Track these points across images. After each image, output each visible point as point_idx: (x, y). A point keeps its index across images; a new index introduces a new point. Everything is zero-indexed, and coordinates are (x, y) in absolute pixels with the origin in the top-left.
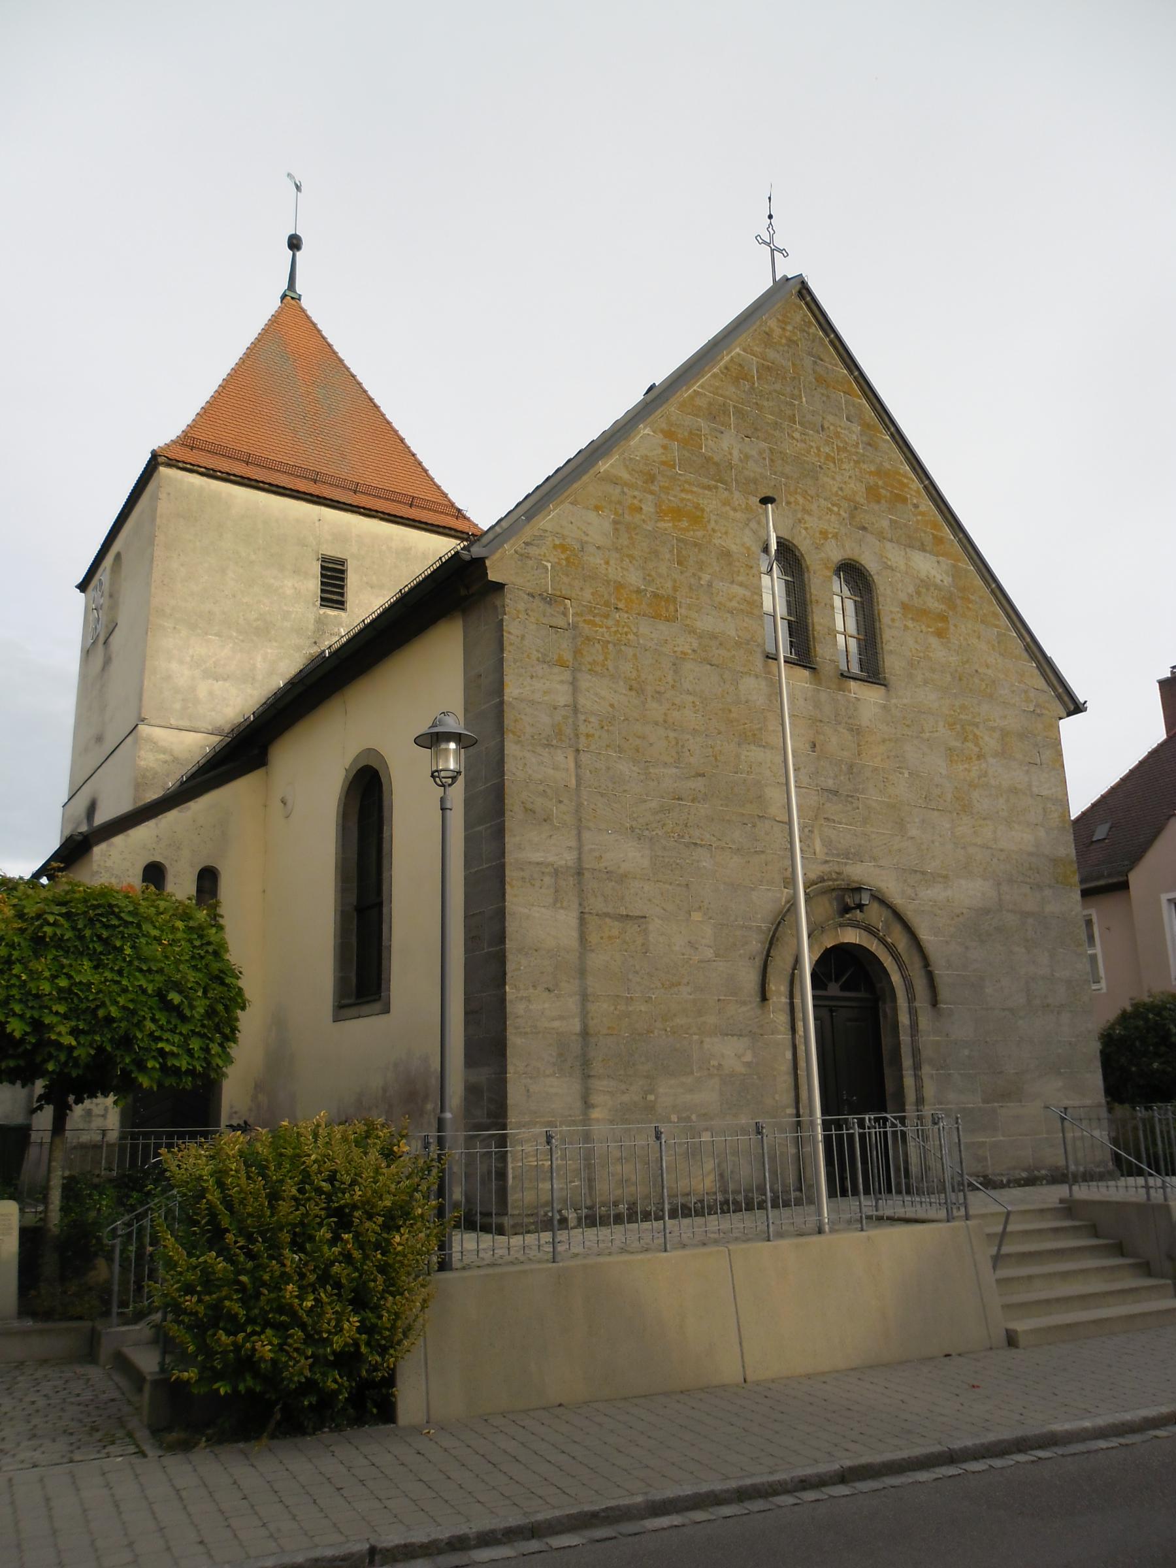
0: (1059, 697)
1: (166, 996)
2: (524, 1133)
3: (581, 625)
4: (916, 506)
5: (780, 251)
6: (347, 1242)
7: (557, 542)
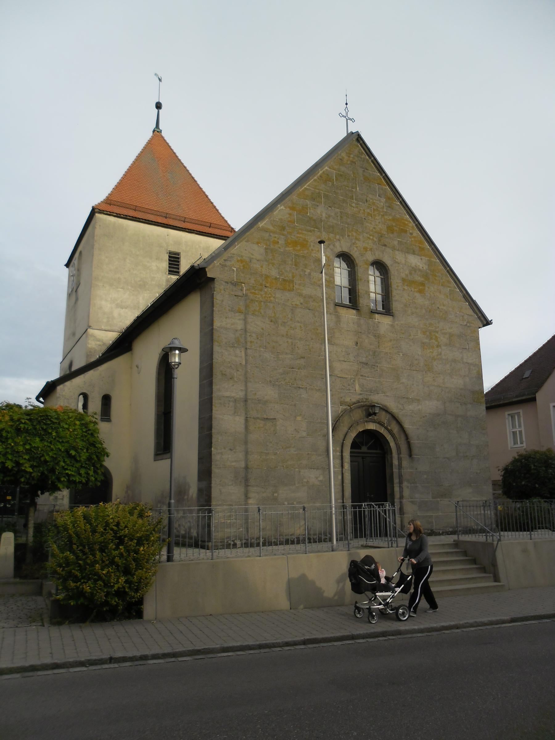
0: (479, 318)
1: (69, 452)
2: (219, 508)
3: (249, 294)
4: (411, 234)
5: (351, 119)
6: (121, 549)
7: (239, 259)
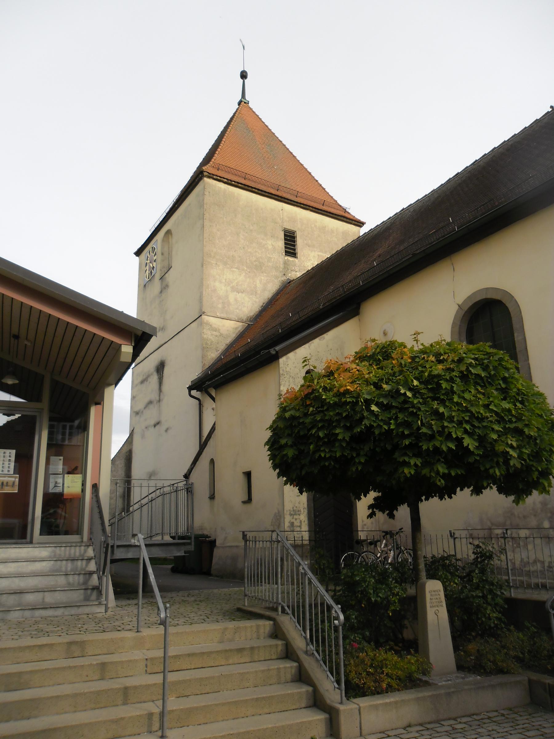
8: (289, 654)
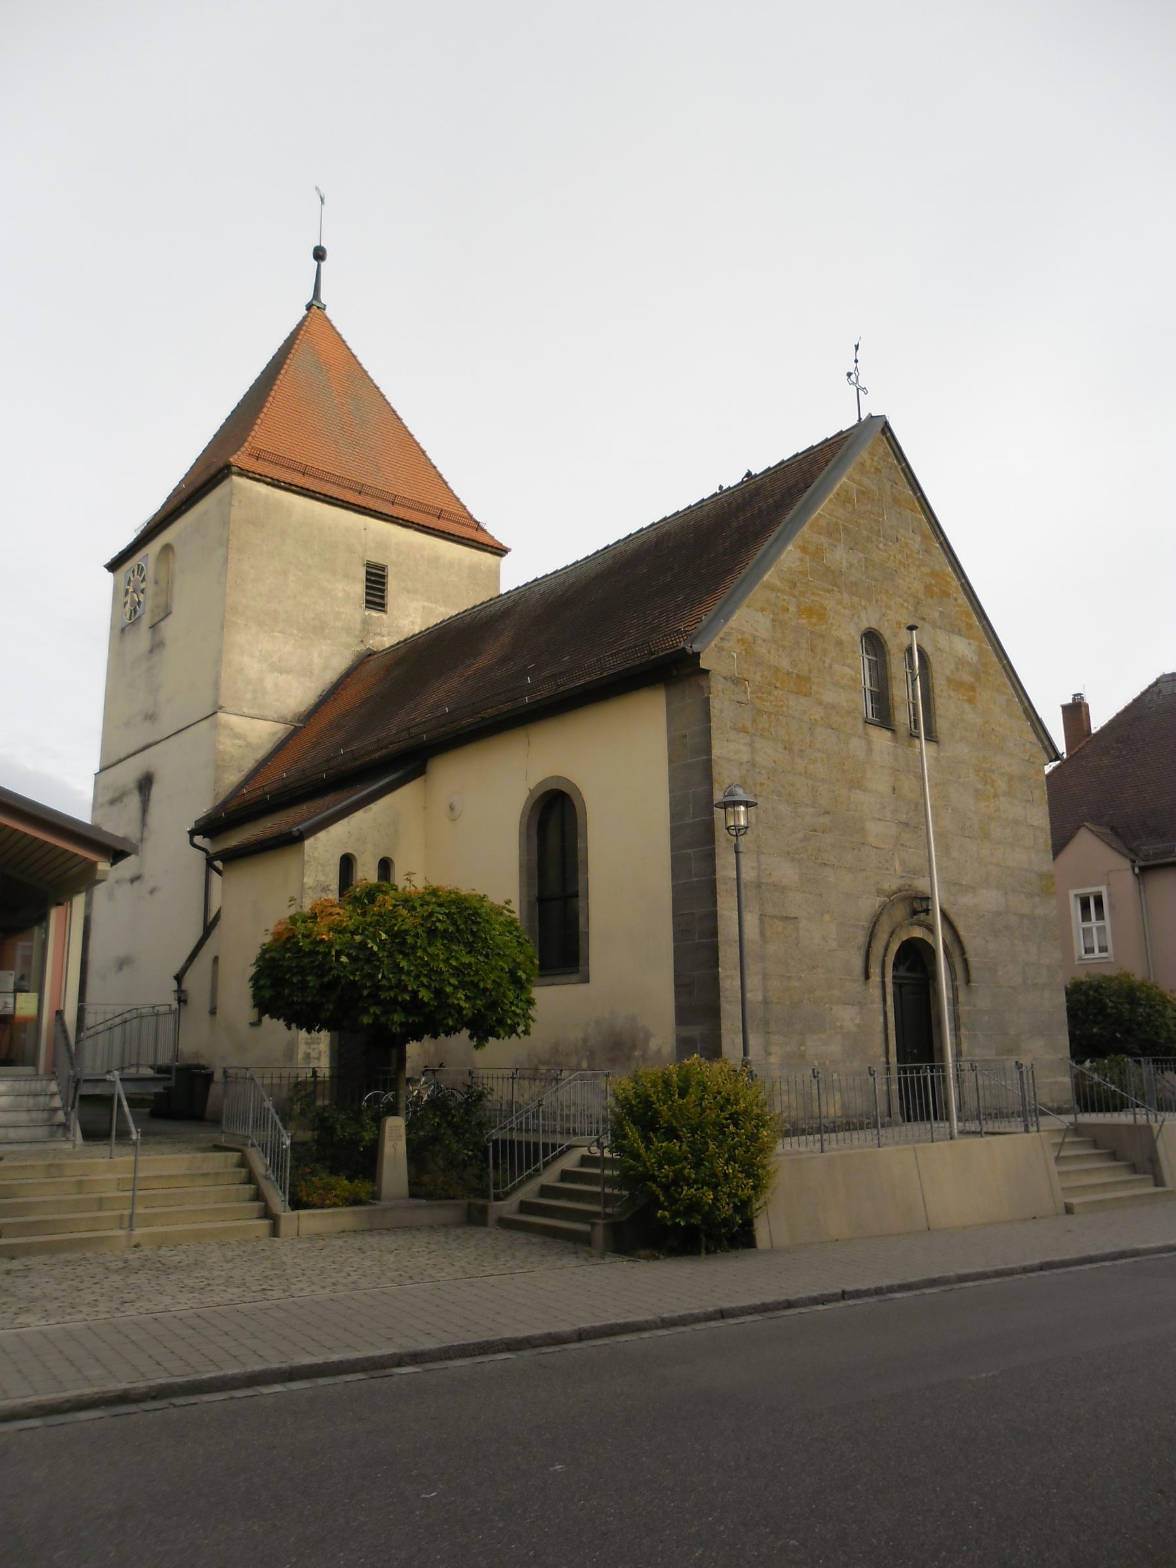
0: (1045, 748)
4: (956, 600)
8: (251, 1179)
